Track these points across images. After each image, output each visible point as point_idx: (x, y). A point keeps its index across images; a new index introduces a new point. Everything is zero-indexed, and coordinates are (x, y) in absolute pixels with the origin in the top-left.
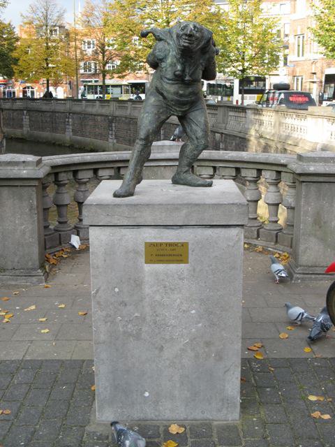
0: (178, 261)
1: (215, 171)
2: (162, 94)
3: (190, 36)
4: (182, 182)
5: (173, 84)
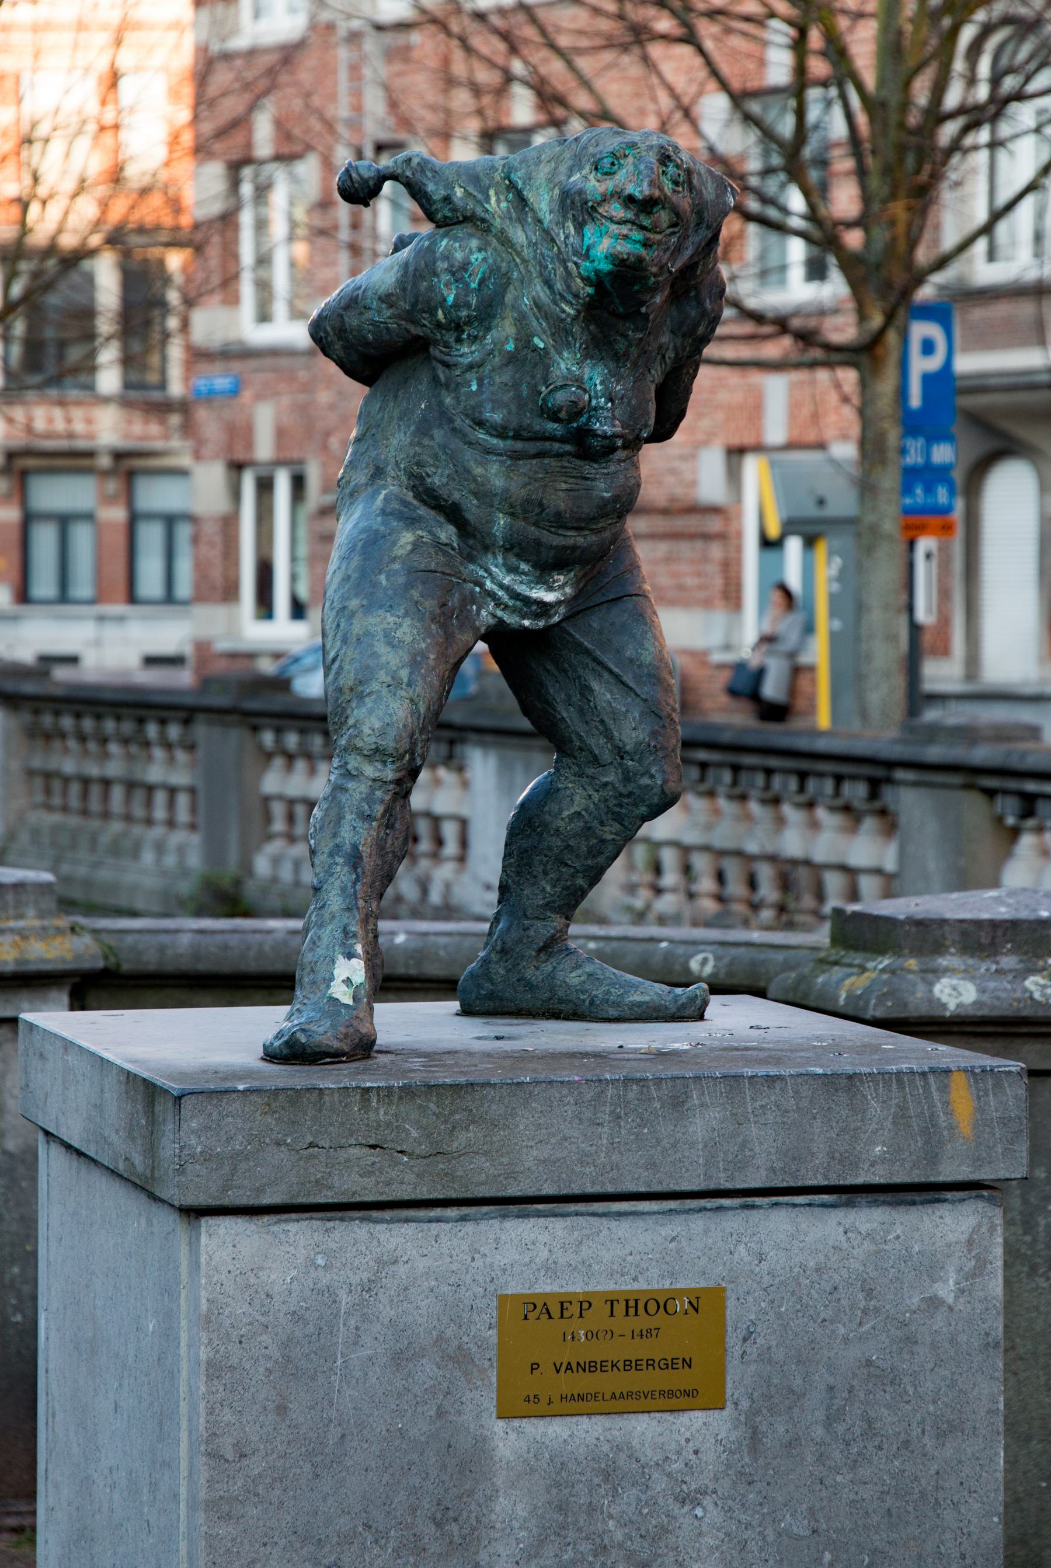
0: (671, 1394)
1: (1028, 812)
2: (453, 513)
3: (647, 205)
4: (613, 1012)
5: (516, 456)
